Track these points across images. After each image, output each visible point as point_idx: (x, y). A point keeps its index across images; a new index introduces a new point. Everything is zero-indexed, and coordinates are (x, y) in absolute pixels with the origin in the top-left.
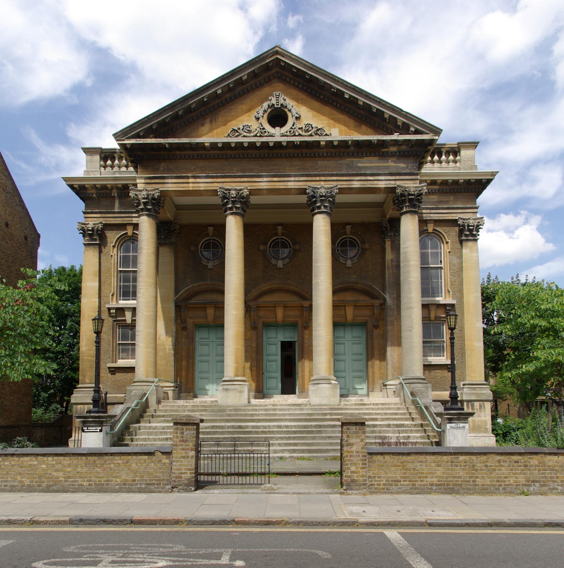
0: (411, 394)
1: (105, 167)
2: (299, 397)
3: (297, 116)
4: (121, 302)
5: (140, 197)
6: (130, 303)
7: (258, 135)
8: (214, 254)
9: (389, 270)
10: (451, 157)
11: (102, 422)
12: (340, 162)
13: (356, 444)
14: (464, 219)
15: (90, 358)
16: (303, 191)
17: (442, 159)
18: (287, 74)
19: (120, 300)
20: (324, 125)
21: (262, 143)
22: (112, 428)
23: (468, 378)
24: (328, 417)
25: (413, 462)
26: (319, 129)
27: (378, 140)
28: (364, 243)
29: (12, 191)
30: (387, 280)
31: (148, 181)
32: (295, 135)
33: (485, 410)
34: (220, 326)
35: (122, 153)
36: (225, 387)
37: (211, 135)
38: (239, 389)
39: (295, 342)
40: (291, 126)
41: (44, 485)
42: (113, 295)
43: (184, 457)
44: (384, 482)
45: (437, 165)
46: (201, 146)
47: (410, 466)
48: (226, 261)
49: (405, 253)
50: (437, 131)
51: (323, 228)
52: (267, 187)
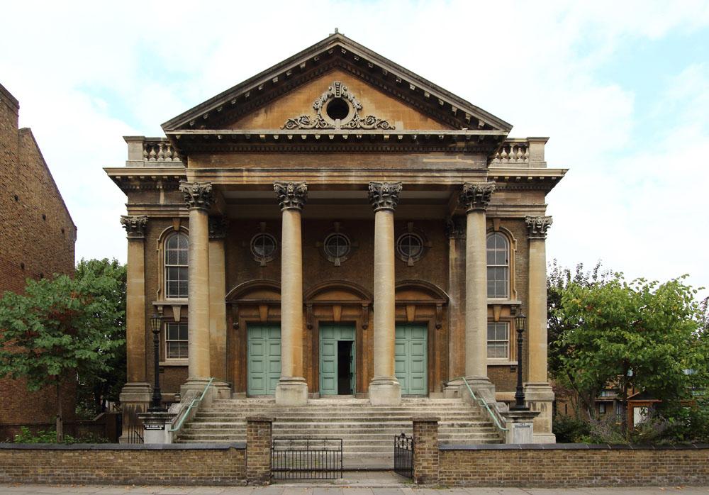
0: (475, 394)
1: (148, 157)
2: (356, 397)
3: (359, 107)
4: (169, 299)
5: (190, 191)
6: (183, 300)
7: (317, 127)
8: (266, 252)
9: (452, 269)
10: (520, 153)
11: (165, 420)
12: (405, 157)
13: (428, 442)
14: (532, 218)
15: (137, 356)
16: (364, 187)
17: (510, 154)
18: (349, 62)
19: (167, 297)
20: (388, 118)
21: (322, 135)
22: (173, 428)
23: (530, 379)
24: (390, 417)
25: (483, 458)
26: (382, 122)
27: (445, 136)
28: (427, 241)
29: (48, 182)
30: (450, 279)
31: (199, 174)
32: (356, 128)
33: (546, 410)
34: (276, 325)
35: (168, 142)
36: (283, 387)
37: (261, 125)
38: (298, 389)
39: (351, 342)
40: (352, 118)
41: (122, 478)
42: (159, 293)
43: (258, 454)
44: (455, 477)
45: (505, 160)
46: (255, 138)
47: (480, 462)
48: (282, 259)
49: (472, 253)
50: (508, 127)
51: (386, 226)
52: (326, 182)
